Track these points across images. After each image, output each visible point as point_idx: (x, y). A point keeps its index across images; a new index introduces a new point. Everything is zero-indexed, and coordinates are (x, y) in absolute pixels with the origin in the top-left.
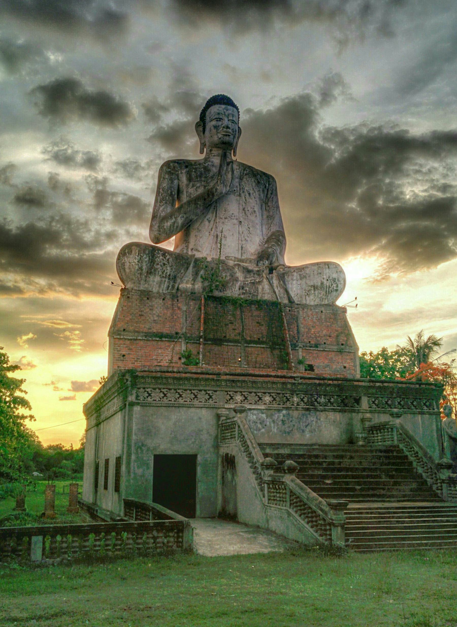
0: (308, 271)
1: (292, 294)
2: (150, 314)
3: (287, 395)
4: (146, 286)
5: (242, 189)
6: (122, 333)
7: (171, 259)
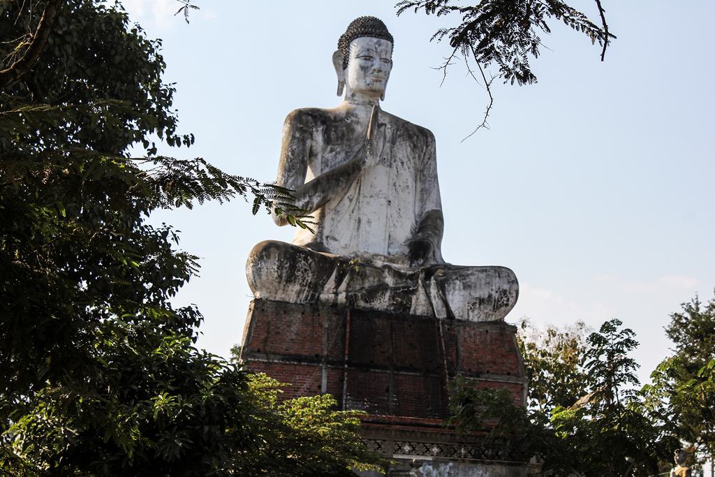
0: (473, 279)
1: (453, 307)
2: (288, 331)
3: (455, 447)
4: (283, 296)
5: (393, 156)
6: (257, 355)
7: (313, 264)
